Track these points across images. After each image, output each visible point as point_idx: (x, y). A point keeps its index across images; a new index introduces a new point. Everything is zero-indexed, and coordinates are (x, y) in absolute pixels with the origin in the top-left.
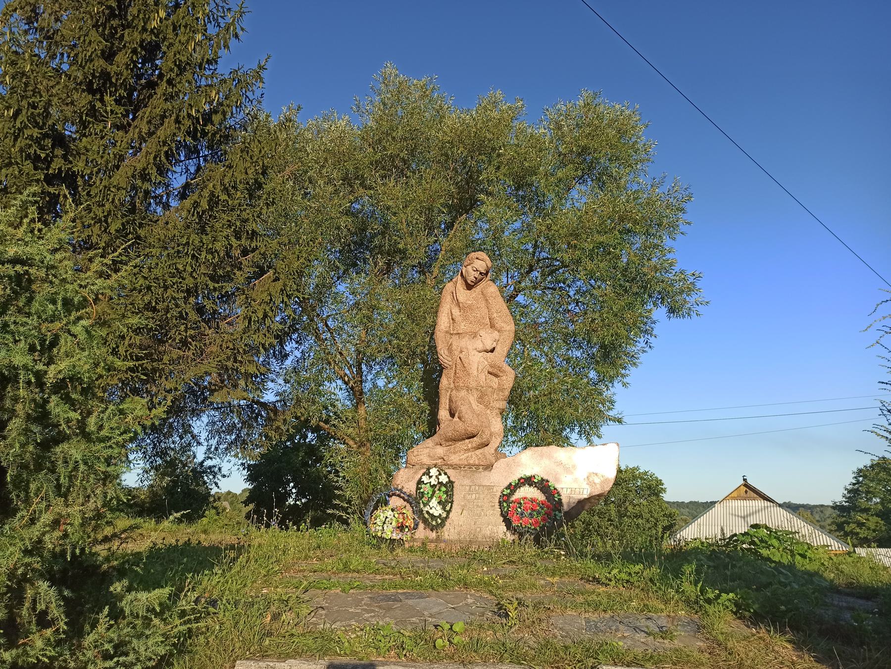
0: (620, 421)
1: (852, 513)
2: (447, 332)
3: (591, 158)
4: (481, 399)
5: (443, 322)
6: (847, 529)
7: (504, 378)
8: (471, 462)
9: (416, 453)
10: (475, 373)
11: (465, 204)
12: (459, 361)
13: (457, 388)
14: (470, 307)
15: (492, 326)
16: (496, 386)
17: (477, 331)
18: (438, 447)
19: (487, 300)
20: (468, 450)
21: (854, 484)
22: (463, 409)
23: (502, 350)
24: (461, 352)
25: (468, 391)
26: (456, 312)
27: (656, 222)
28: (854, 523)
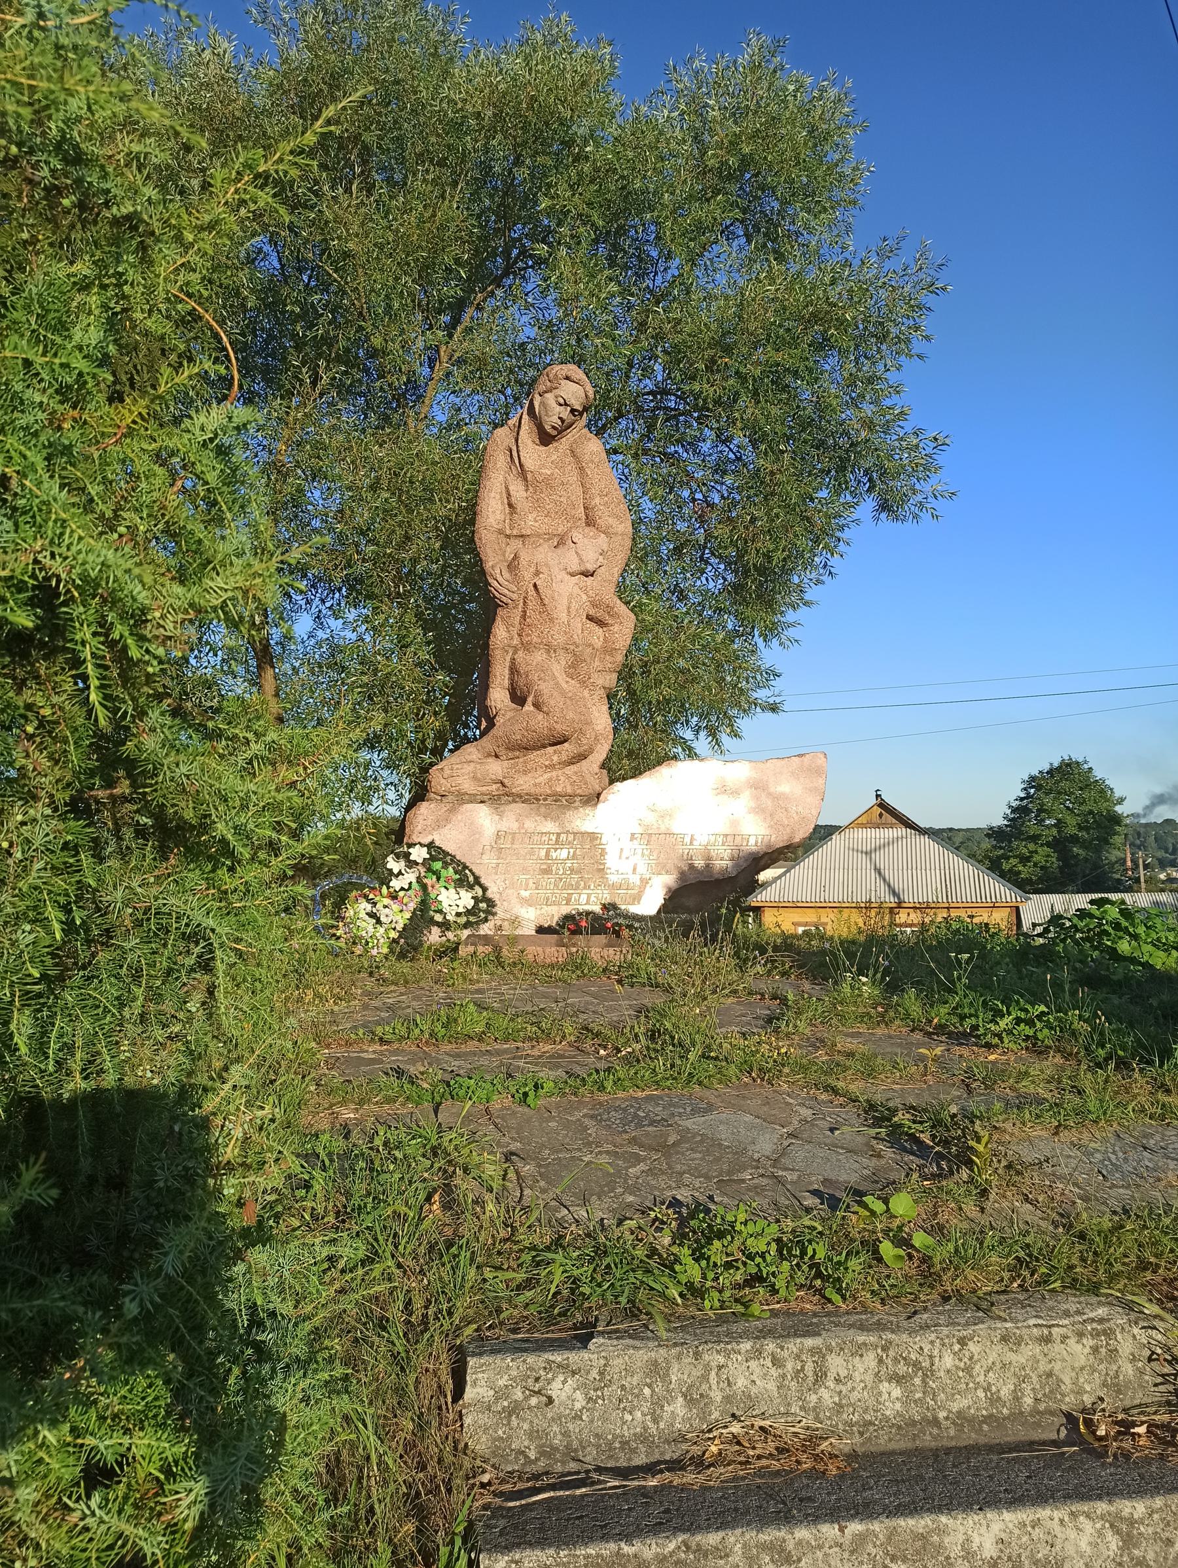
0: (774, 708)
1: (1015, 844)
2: (500, 532)
3: (759, 190)
4: (574, 669)
5: (492, 512)
6: (1006, 866)
7: (616, 628)
8: (559, 789)
9: (447, 772)
10: (563, 617)
11: (496, 261)
12: (532, 592)
13: (527, 647)
14: (548, 482)
15: (590, 522)
16: (598, 644)
17: (562, 530)
18: (491, 760)
19: (581, 469)
20: (552, 767)
21: (1022, 799)
22: (545, 687)
23: (611, 573)
24: (537, 573)
25: (548, 652)
26: (518, 490)
27: (866, 332)
28: (1015, 857)
